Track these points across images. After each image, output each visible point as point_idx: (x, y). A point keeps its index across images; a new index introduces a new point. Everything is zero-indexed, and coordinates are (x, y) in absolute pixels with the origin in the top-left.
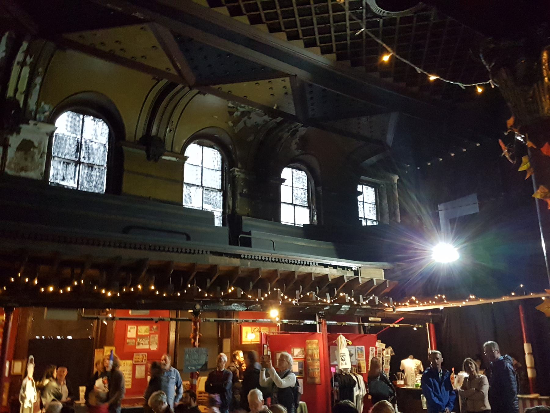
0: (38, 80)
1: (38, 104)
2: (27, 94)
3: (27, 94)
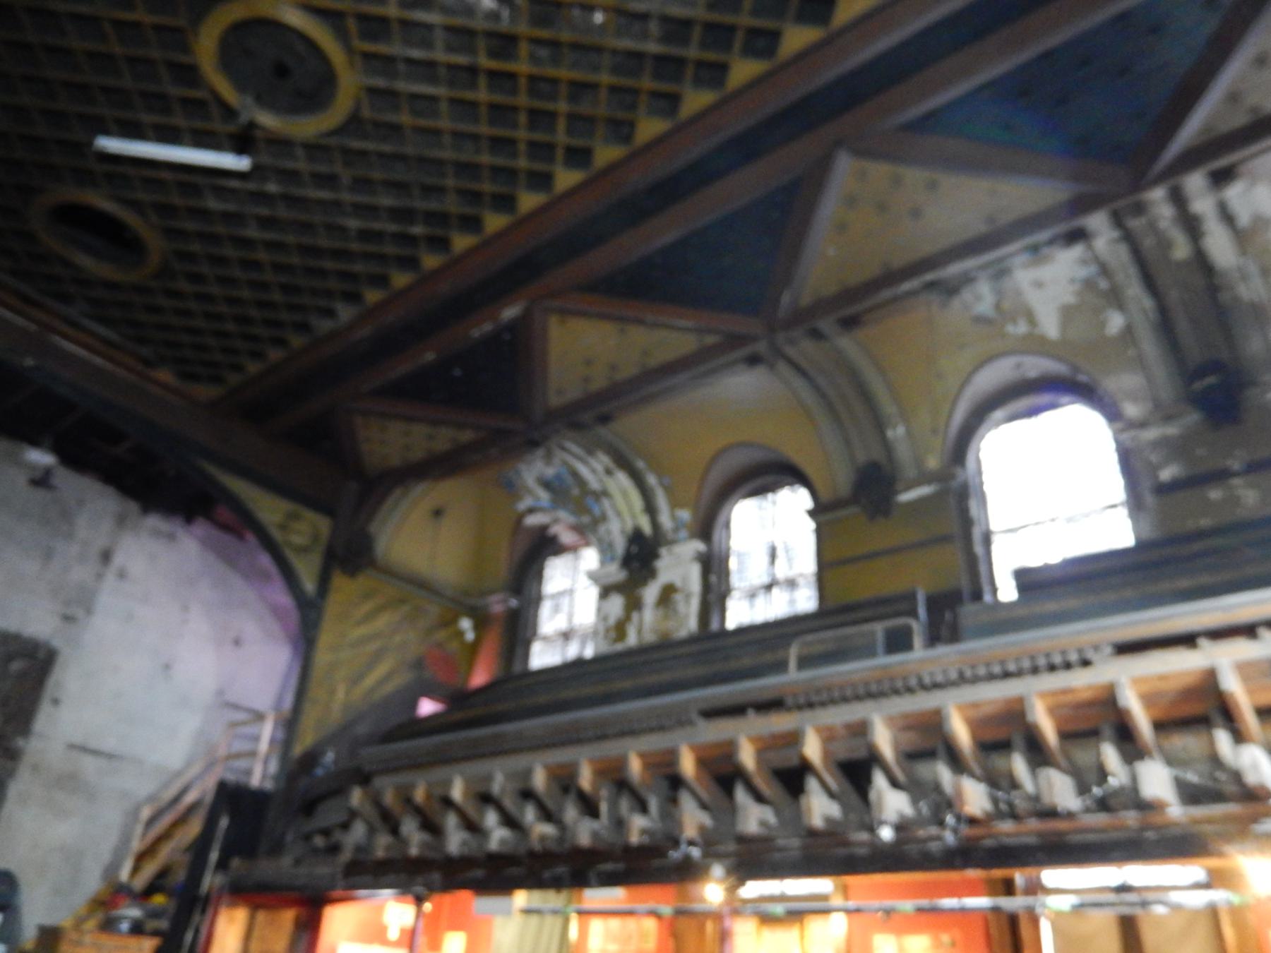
0: (652, 480)
1: (673, 517)
2: (651, 509)
3: (651, 509)
